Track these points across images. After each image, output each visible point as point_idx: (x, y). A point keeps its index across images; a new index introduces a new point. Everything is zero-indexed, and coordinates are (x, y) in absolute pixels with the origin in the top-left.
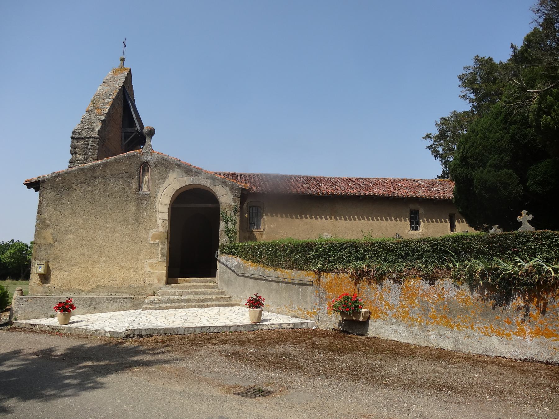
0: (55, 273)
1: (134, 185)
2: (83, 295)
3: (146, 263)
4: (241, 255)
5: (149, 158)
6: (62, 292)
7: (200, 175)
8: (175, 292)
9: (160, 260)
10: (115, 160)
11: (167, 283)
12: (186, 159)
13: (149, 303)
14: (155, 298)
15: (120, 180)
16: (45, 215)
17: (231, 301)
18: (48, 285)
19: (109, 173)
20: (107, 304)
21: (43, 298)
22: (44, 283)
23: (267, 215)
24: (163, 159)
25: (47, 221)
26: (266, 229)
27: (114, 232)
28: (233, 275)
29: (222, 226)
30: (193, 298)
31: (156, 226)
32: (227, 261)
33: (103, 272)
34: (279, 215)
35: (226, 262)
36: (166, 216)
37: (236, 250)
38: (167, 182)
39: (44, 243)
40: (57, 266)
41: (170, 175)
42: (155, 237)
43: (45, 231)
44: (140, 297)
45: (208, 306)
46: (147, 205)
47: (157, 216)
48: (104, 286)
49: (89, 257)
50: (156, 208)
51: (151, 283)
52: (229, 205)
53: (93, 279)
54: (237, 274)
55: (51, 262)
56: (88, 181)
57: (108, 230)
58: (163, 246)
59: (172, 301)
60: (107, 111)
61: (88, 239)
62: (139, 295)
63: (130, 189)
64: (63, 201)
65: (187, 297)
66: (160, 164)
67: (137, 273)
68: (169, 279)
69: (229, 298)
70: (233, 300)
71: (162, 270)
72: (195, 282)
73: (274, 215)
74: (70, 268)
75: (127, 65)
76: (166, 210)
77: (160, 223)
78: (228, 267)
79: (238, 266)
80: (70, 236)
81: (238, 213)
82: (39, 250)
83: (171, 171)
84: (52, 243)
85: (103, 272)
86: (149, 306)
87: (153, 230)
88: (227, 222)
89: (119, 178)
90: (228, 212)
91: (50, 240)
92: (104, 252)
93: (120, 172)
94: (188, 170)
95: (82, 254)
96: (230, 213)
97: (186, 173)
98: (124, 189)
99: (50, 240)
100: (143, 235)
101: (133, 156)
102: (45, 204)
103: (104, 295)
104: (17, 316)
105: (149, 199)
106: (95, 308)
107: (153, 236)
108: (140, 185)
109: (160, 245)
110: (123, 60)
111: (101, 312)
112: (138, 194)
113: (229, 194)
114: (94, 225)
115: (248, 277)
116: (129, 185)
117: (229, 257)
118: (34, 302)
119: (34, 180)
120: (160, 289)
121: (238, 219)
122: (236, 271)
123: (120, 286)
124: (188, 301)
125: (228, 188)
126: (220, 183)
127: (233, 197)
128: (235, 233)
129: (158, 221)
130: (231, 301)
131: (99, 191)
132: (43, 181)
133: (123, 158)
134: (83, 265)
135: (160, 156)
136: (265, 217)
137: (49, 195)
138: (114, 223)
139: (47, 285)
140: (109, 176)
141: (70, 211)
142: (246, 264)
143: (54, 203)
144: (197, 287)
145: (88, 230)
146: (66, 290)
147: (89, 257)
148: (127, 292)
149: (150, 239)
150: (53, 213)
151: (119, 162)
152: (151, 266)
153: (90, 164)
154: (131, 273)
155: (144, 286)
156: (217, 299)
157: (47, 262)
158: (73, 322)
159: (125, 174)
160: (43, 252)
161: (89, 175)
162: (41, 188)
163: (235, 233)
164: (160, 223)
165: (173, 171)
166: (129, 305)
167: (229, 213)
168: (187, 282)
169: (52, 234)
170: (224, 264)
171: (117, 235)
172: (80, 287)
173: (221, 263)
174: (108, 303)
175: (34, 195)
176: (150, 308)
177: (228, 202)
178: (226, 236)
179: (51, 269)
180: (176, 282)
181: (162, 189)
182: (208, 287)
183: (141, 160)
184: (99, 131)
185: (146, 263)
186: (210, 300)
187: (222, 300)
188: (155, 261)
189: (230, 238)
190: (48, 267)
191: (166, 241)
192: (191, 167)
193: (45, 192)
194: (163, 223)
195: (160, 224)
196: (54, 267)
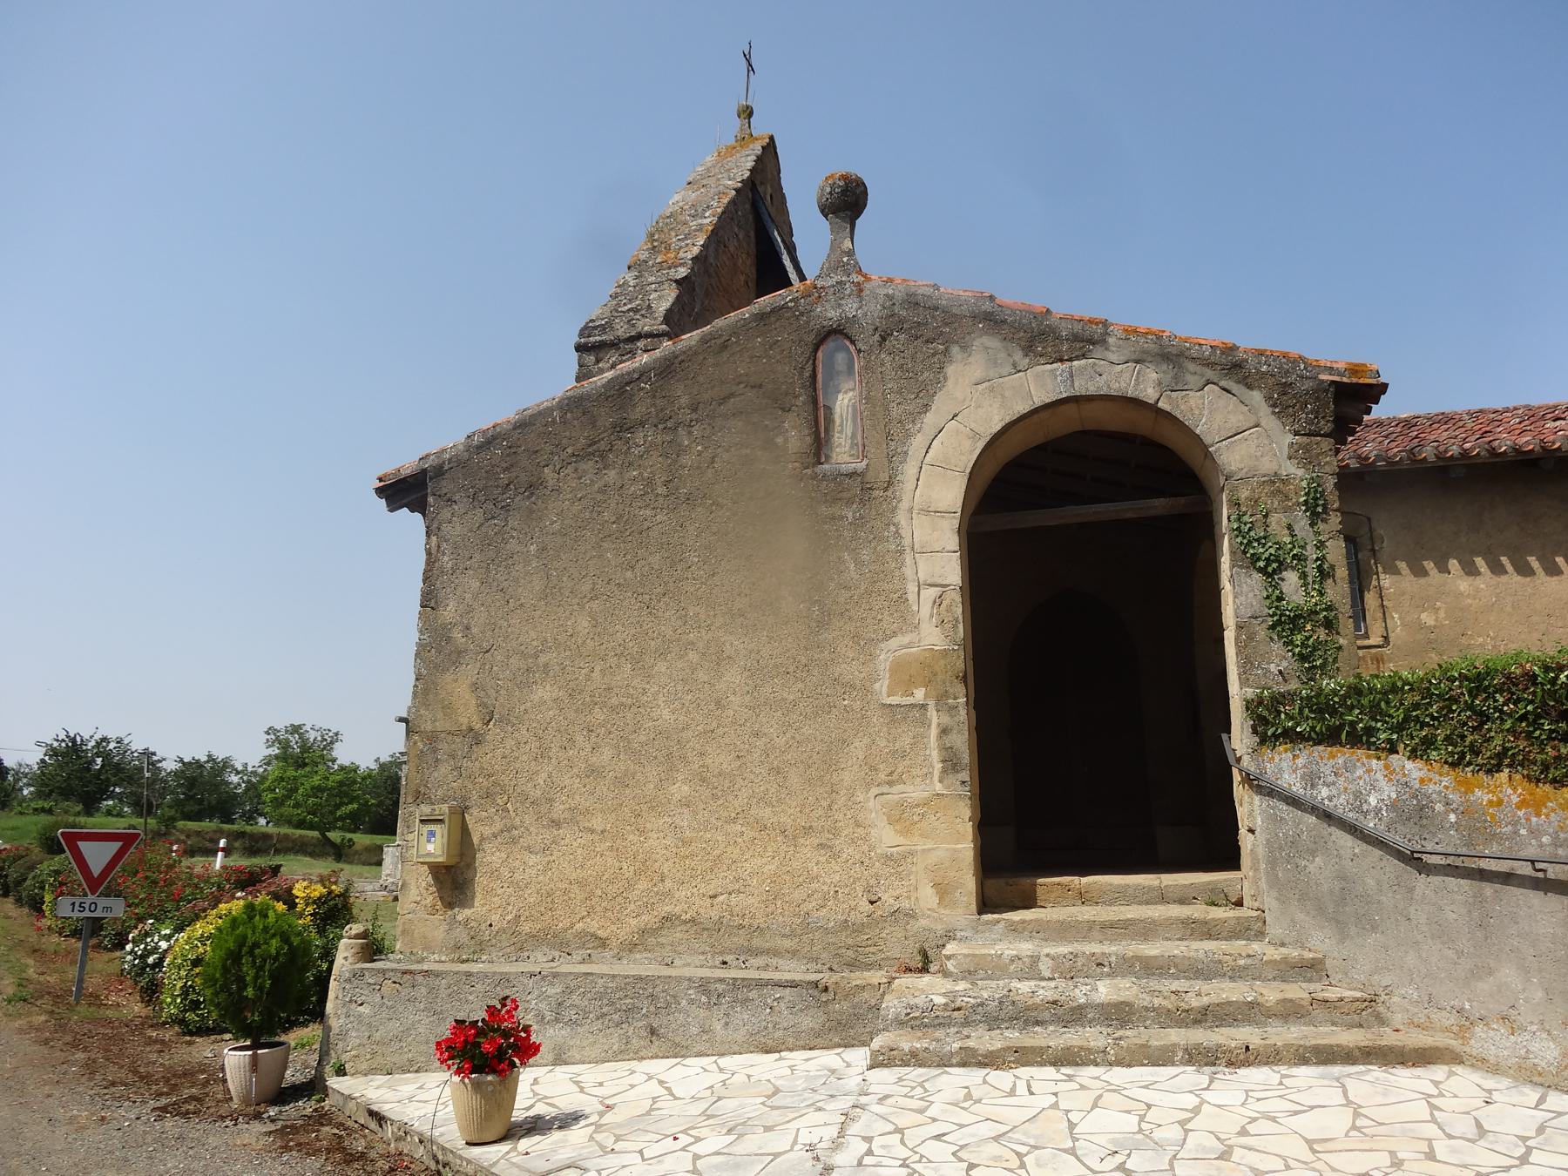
0: (490, 858)
1: (794, 437)
2: (603, 966)
3: (873, 807)
4: (1428, 743)
5: (851, 307)
6: (521, 946)
7: (1098, 351)
8: (1035, 959)
9: (939, 788)
10: (705, 340)
11: (987, 904)
12: (1019, 291)
13: (913, 1021)
14: (932, 989)
16: (449, 612)
17: (1381, 1020)
18: (467, 912)
19: (684, 400)
20: (703, 1013)
21: (437, 975)
22: (450, 905)
23: (1396, 571)
24: (912, 302)
25: (457, 634)
26: (1398, 633)
27: (720, 660)
28: (1377, 870)
29: (1238, 596)
30: (1145, 1000)
31: (907, 622)
32: (1312, 779)
33: (684, 851)
34: (1453, 564)
35: (1273, 786)
36: (951, 571)
37: (1375, 711)
38: (941, 405)
39: (448, 726)
40: (498, 826)
41: (950, 370)
42: (904, 676)
43: (448, 677)
44: (858, 978)
45: (1247, 1057)
47: (908, 571)
48: (693, 920)
49: (621, 782)
51: (905, 904)
52: (1276, 483)
53: (642, 885)
54: (1413, 860)
55: (474, 811)
56: (603, 445)
57: (693, 656)
58: (946, 719)
59: (1027, 1016)
60: (696, 250)
61: (614, 701)
62: (853, 965)
64: (513, 545)
65: (1105, 991)
67: (836, 856)
68: (989, 882)
69: (1368, 1009)
70: (1398, 1019)
71: (952, 840)
72: (1123, 897)
73: (1429, 565)
74: (548, 835)
76: (951, 541)
77: (923, 604)
78: (1327, 817)
79: (1417, 811)
80: (544, 692)
81: (1335, 520)
82: (430, 758)
83: (955, 349)
84: (478, 726)
85: (684, 851)
86: (907, 1042)
87: (894, 643)
88: (1271, 570)
90: (1274, 519)
91: (468, 715)
92: (683, 758)
94: (1038, 337)
95: (594, 772)
96: (1287, 525)
97: (1028, 349)
99: (468, 715)
100: (850, 670)
101: (777, 311)
102: (446, 561)
103: (693, 966)
104: (345, 1057)
105: (866, 494)
106: (653, 1032)
107: (897, 668)
108: (817, 433)
109: (932, 714)
110: (747, 113)
111: (678, 1051)
112: (815, 477)
113: (1270, 422)
114: (634, 637)
115: (1507, 878)
117: (1329, 759)
118: (404, 992)
119: (405, 472)
120: (949, 936)
121: (1336, 551)
122: (1397, 839)
123: (760, 921)
124: (1118, 1014)
125: (1257, 396)
126: (1209, 374)
127: (1290, 438)
128: (1329, 624)
129: (912, 597)
130: (1381, 1020)
131: (650, 482)
132: (439, 471)
133: (734, 331)
134: (597, 823)
135: (898, 292)
136: (1386, 581)
137: (460, 522)
138: (720, 621)
139: (463, 914)
140: (685, 415)
141: (538, 584)
142: (1481, 796)
143: (477, 557)
144: (1147, 930)
145: (613, 661)
146: (542, 938)
147: (621, 782)
148: (794, 953)
149: (882, 686)
150: (475, 598)
151: (724, 346)
152: (900, 817)
153: (609, 375)
154: (807, 855)
155: (873, 921)
156: (1290, 1012)
157: (461, 812)
158: (536, 1126)
159: (751, 394)
160: (444, 769)
161: (606, 419)
162: (431, 499)
163: (1329, 624)
164: (923, 604)
165: (964, 348)
166: (808, 1022)
167: (1277, 522)
168: (1083, 898)
169: (475, 687)
170: (1294, 802)
171: (733, 676)
172: (593, 925)
173: (1268, 791)
174: (709, 1006)
175: (410, 523)
176: (914, 1054)
177: (1267, 466)
178: (1277, 647)
179: (476, 840)
180: (1029, 902)
181: (918, 442)
182: (1207, 931)
183: (815, 325)
184: (669, 312)
185: (873, 807)
186: (1250, 1012)
187: (1318, 1013)
188: (915, 792)
189: (1303, 658)
190: (465, 831)
191: (960, 689)
192: (1053, 321)
193: (446, 514)
194: (938, 602)
195: (926, 610)
196: (487, 831)
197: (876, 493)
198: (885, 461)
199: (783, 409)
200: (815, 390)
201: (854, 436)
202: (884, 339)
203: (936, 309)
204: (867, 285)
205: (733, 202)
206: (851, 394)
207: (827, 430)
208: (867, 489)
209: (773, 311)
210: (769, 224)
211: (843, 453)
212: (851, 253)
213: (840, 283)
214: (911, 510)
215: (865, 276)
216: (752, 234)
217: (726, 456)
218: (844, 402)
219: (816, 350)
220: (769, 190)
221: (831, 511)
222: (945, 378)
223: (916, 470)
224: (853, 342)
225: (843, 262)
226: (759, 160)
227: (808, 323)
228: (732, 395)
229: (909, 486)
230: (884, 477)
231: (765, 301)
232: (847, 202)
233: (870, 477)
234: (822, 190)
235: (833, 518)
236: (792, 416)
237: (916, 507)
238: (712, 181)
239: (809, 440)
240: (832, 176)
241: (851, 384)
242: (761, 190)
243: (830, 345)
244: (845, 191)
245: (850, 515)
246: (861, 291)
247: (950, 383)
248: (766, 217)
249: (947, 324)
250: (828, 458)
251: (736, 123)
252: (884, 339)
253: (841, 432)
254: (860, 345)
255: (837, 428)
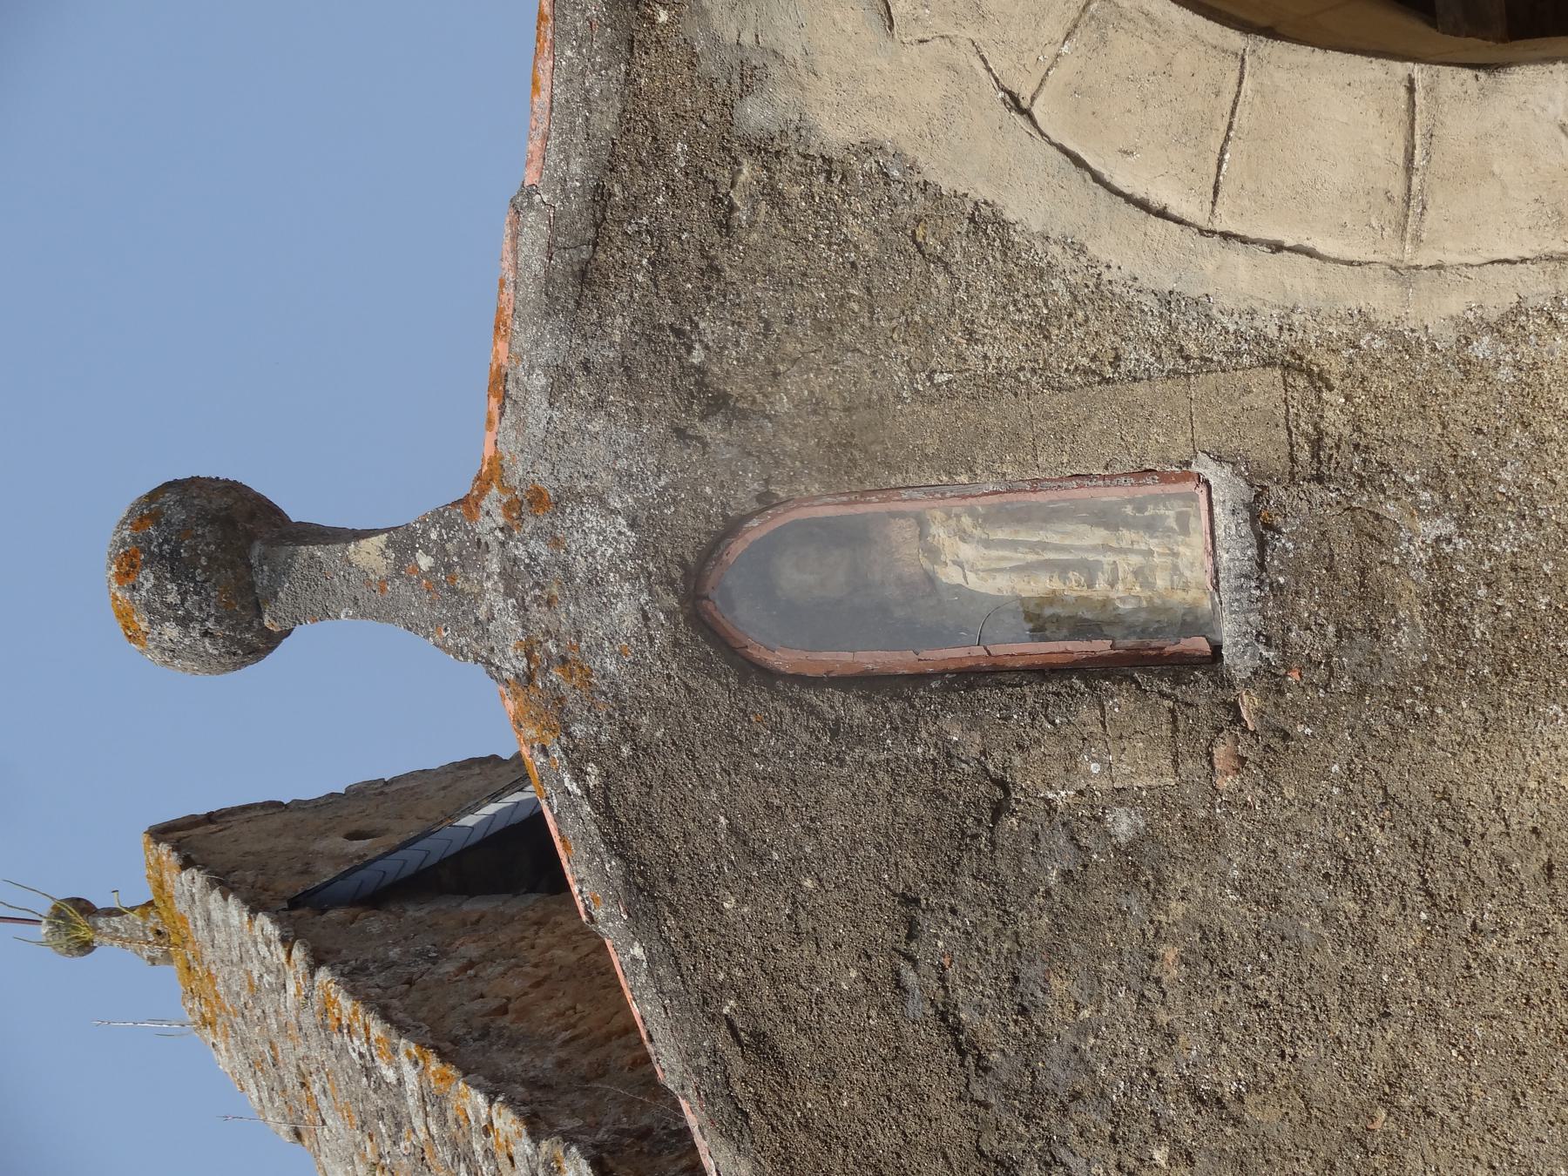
1: (1115, 763)
5: (600, 537)
15: (1056, 1019)
24: (579, 283)
41: (835, 131)
46: (1461, 489)
50: (1506, 326)
60: (507, 1123)
63: (1205, 836)
66: (665, 338)
75: (124, 871)
83: (755, 115)
89: (1032, 1047)
93: (923, 1037)
98: (1209, 950)
101: (617, 833)
110: (76, 921)
112: (1271, 680)
116: (1138, 866)
135: (537, 348)
151: (759, 1046)
159: (939, 939)
165: (749, 78)
181: (1129, 255)
197: (1335, 421)
198: (1204, 384)
199: (999, 810)
200: (919, 678)
201: (1106, 518)
202: (718, 403)
203: (600, 195)
204: (517, 473)
205: (353, 979)
206: (939, 533)
207: (1082, 628)
208: (1317, 461)
209: (619, 846)
210: (436, 847)
211: (1174, 558)
212: (403, 542)
213: (509, 579)
214: (1402, 273)
215: (482, 483)
216: (474, 907)
217: (1193, 1046)
218: (982, 563)
219: (767, 675)
220: (336, 843)
221: (1410, 608)
222: (869, 149)
223: (1237, 257)
224: (733, 527)
225: (435, 570)
226: (223, 881)
227: (660, 710)
228: (946, 1017)
229: (1298, 282)
230: (1265, 388)
231: (587, 877)
232: (219, 559)
233: (1268, 448)
234: (172, 653)
235: (1442, 599)
236: (1025, 775)
237: (1392, 251)
238: (290, 1052)
239: (1120, 703)
240: (124, 616)
241: (902, 532)
242: (327, 872)
243: (747, 620)
244: (175, 564)
245: (1430, 529)
246: (537, 499)
247: (886, 130)
248: (413, 858)
249: (660, 152)
250: (1191, 623)
251: (116, 961)
252: (718, 403)
253: (1090, 571)
254: (744, 499)
255: (1071, 587)
